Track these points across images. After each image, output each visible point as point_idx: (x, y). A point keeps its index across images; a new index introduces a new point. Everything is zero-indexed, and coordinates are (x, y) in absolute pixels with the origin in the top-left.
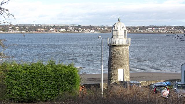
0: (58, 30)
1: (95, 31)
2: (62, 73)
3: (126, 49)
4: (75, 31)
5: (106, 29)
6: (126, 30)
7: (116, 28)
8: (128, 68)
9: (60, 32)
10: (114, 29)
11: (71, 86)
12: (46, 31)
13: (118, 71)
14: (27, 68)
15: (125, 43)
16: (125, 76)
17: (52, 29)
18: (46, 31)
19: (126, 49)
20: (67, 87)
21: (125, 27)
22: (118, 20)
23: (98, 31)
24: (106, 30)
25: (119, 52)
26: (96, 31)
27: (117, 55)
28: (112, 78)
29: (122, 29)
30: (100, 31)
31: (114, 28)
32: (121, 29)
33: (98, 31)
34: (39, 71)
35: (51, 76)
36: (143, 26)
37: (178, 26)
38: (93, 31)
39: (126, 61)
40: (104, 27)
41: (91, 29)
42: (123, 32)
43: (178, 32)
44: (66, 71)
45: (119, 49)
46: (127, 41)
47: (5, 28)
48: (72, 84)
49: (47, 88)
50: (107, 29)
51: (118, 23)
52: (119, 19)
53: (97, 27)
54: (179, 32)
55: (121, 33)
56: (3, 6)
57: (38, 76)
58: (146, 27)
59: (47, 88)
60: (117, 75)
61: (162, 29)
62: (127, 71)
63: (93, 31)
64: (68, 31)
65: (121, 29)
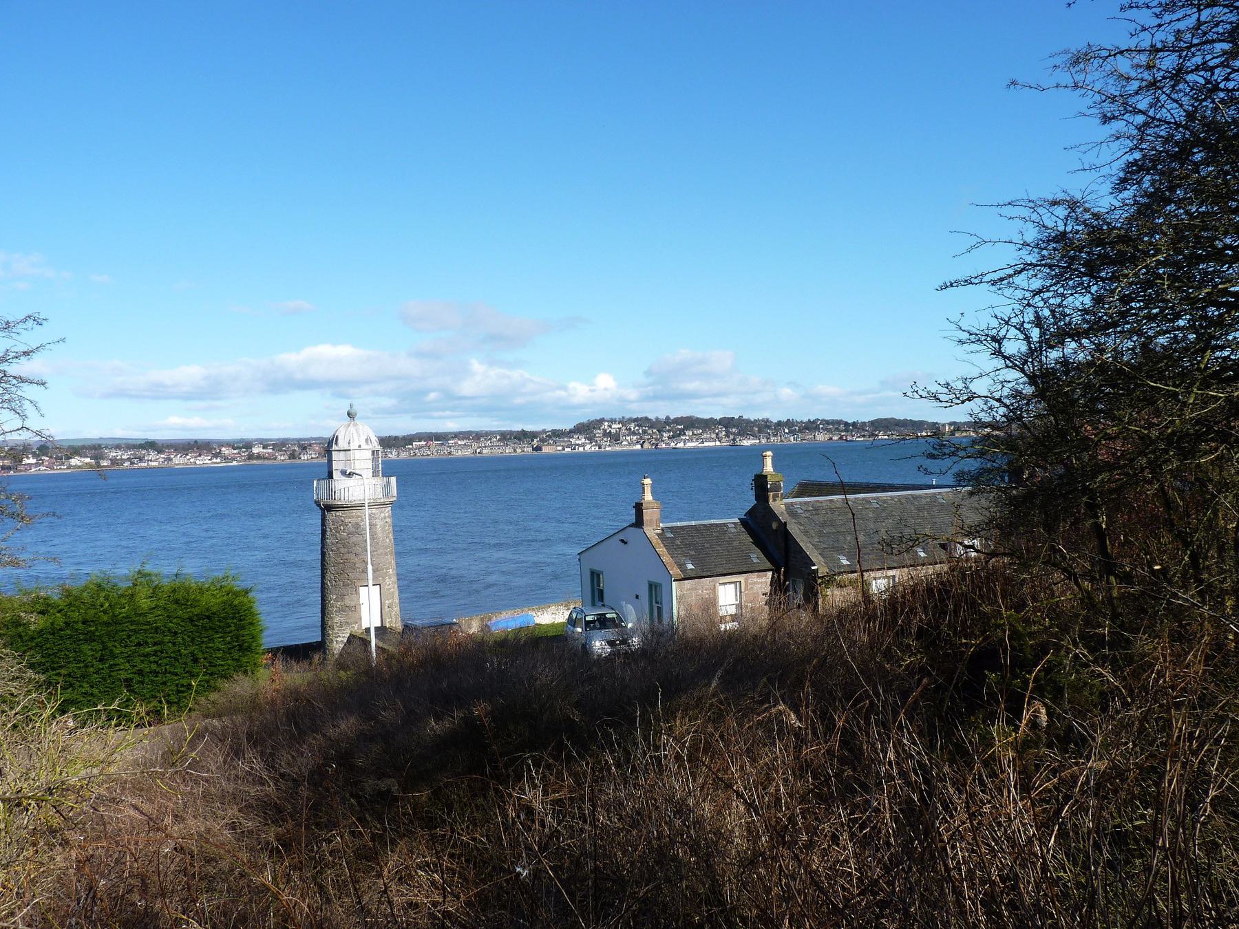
0: (63, 464)
1: (214, 460)
2: (197, 611)
3: (382, 515)
4: (132, 463)
5: (256, 450)
6: (378, 447)
7: (342, 444)
8: (394, 578)
9: (69, 471)
10: (335, 447)
11: (236, 655)
12: (9, 468)
13: (357, 593)
14: (48, 605)
15: (379, 495)
16: (386, 609)
17: (32, 461)
18: (9, 468)
19: (382, 515)
20: (220, 662)
21: (374, 439)
22: (349, 414)
23: (225, 459)
24: (258, 454)
25: (357, 525)
26: (218, 460)
27: (354, 539)
28: (337, 619)
29: (364, 446)
30: (233, 459)
31: (336, 443)
32: (360, 446)
33: (225, 459)
34: (105, 612)
35: (157, 630)
36: (394, 434)
37: (511, 431)
38: (204, 461)
39: (386, 554)
40: (248, 445)
41: (200, 455)
42: (368, 454)
43: (515, 450)
44: (212, 601)
45: (358, 517)
46: (387, 486)
47: (16, 454)
48: (241, 648)
49: (140, 672)
50: (261, 450)
51: (349, 425)
52: (352, 411)
53: (221, 444)
54: (519, 450)
55: (363, 461)
56: (13, 369)
57: (102, 631)
58: (404, 438)
59: (140, 672)
60: (355, 608)
61: (459, 442)
62: (390, 589)
63: (207, 461)
64: (105, 463)
65: (360, 446)
